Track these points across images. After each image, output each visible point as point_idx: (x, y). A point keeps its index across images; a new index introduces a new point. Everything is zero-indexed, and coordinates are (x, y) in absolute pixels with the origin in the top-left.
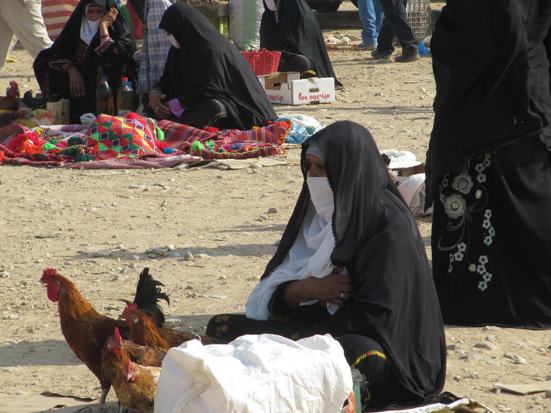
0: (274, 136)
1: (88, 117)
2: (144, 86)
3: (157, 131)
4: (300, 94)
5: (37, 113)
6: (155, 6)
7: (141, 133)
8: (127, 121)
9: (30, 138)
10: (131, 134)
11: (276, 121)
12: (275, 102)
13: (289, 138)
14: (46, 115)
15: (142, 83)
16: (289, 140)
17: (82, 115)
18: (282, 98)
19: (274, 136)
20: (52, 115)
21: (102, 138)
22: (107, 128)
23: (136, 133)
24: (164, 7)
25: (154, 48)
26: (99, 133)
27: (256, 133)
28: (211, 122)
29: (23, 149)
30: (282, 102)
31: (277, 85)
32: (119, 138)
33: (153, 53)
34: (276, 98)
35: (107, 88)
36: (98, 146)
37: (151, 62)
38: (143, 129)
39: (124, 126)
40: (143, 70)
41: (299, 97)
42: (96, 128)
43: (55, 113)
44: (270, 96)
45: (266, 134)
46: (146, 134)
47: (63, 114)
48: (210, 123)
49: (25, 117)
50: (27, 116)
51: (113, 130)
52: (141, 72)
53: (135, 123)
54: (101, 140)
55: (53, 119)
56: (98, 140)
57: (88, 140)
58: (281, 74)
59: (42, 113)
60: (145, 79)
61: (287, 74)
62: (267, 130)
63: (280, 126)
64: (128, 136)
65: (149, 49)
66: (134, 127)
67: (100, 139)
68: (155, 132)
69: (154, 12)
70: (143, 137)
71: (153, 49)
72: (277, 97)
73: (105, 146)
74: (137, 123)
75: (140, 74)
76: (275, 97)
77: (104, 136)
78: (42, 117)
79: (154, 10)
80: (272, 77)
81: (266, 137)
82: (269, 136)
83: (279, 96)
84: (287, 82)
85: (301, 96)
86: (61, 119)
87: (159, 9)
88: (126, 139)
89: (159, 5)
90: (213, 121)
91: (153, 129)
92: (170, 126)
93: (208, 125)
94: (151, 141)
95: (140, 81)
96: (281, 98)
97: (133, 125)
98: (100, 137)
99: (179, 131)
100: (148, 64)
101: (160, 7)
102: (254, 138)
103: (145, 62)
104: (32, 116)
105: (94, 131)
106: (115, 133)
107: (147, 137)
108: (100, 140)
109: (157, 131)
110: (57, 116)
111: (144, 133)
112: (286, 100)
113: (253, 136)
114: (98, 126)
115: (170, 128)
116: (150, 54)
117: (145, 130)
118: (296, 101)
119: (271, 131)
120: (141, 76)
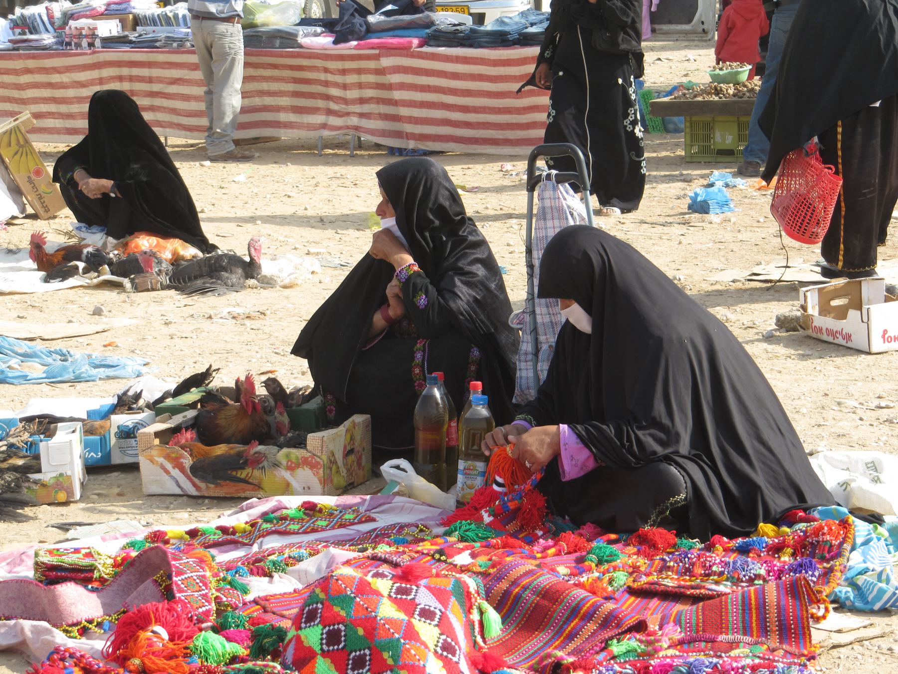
0: (798, 613)
1: (398, 467)
2: (528, 388)
3: (481, 613)
4: (885, 332)
5: (287, 455)
6: (549, 216)
7: (428, 632)
8: (400, 591)
9: (158, 621)
10: (398, 640)
11: (816, 514)
12: (836, 341)
13: (845, 591)
14: (305, 462)
15: (524, 381)
16: (843, 596)
17: (383, 464)
18: (850, 336)
19: (798, 613)
20: (317, 463)
21: (328, 644)
22: (343, 613)
23: (411, 634)
24: (567, 219)
25: (547, 307)
26: (320, 627)
27: (753, 602)
28: (657, 516)
29: (134, 656)
30: (849, 344)
31: (841, 313)
32: (369, 648)
33: (547, 319)
34: (838, 335)
35: (437, 404)
36: (314, 667)
37: (542, 338)
38: (435, 622)
39: (387, 610)
40: (526, 354)
41: (883, 337)
42: (317, 609)
43: (325, 458)
44: (827, 329)
45: (778, 602)
46: (444, 637)
47: (348, 453)
48: (653, 517)
49: (261, 466)
50: (265, 463)
51: (356, 623)
52: (523, 358)
53: (417, 601)
54: (325, 647)
55: (321, 471)
56: (317, 649)
57: (293, 642)
58: (848, 282)
59: (297, 458)
60: (531, 374)
61: (860, 282)
62: (782, 592)
63: (824, 534)
64: (393, 645)
65: (538, 310)
66: (411, 615)
67: (322, 644)
68: (475, 616)
69: (546, 228)
70: (432, 647)
71: (544, 310)
72: (841, 333)
73: (333, 667)
74: (424, 598)
75: (520, 361)
76: (836, 332)
77: (332, 637)
78: (298, 466)
79: (545, 224)
80: (832, 288)
81: (779, 613)
82: (786, 610)
83: (844, 333)
84: (860, 309)
85: (886, 336)
86: (345, 465)
87: (557, 223)
88: (386, 655)
89: (556, 215)
90: (662, 512)
91: (471, 607)
92: (525, 581)
93: (650, 522)
94: (455, 659)
95: (521, 377)
96: (848, 337)
97: (409, 607)
98: (322, 639)
99: (546, 603)
100: (536, 342)
101: (559, 219)
102: (746, 595)
103: (529, 337)
104: (276, 465)
105: (311, 617)
106: (361, 631)
107: (447, 647)
108: (322, 649)
109: (481, 613)
110: (333, 462)
111: (437, 631)
112: (858, 341)
113: (743, 610)
114: (322, 603)
115: (525, 588)
116: (539, 319)
117: (444, 625)
118: (877, 345)
119: (793, 597)
120: (523, 365)
